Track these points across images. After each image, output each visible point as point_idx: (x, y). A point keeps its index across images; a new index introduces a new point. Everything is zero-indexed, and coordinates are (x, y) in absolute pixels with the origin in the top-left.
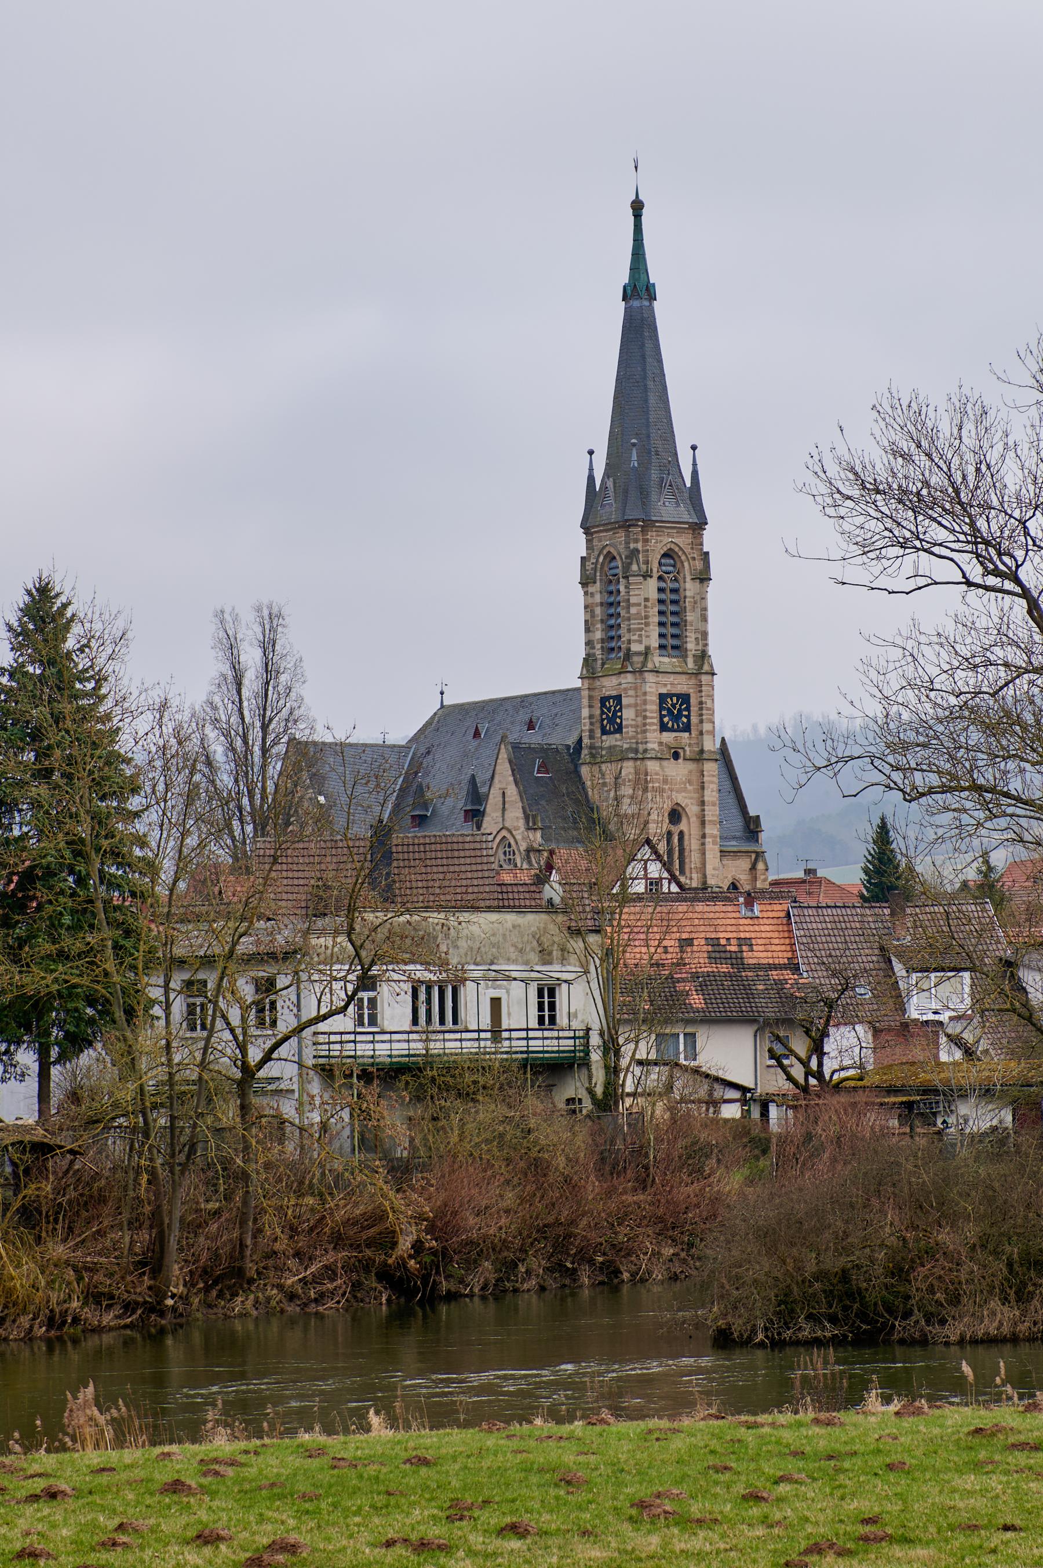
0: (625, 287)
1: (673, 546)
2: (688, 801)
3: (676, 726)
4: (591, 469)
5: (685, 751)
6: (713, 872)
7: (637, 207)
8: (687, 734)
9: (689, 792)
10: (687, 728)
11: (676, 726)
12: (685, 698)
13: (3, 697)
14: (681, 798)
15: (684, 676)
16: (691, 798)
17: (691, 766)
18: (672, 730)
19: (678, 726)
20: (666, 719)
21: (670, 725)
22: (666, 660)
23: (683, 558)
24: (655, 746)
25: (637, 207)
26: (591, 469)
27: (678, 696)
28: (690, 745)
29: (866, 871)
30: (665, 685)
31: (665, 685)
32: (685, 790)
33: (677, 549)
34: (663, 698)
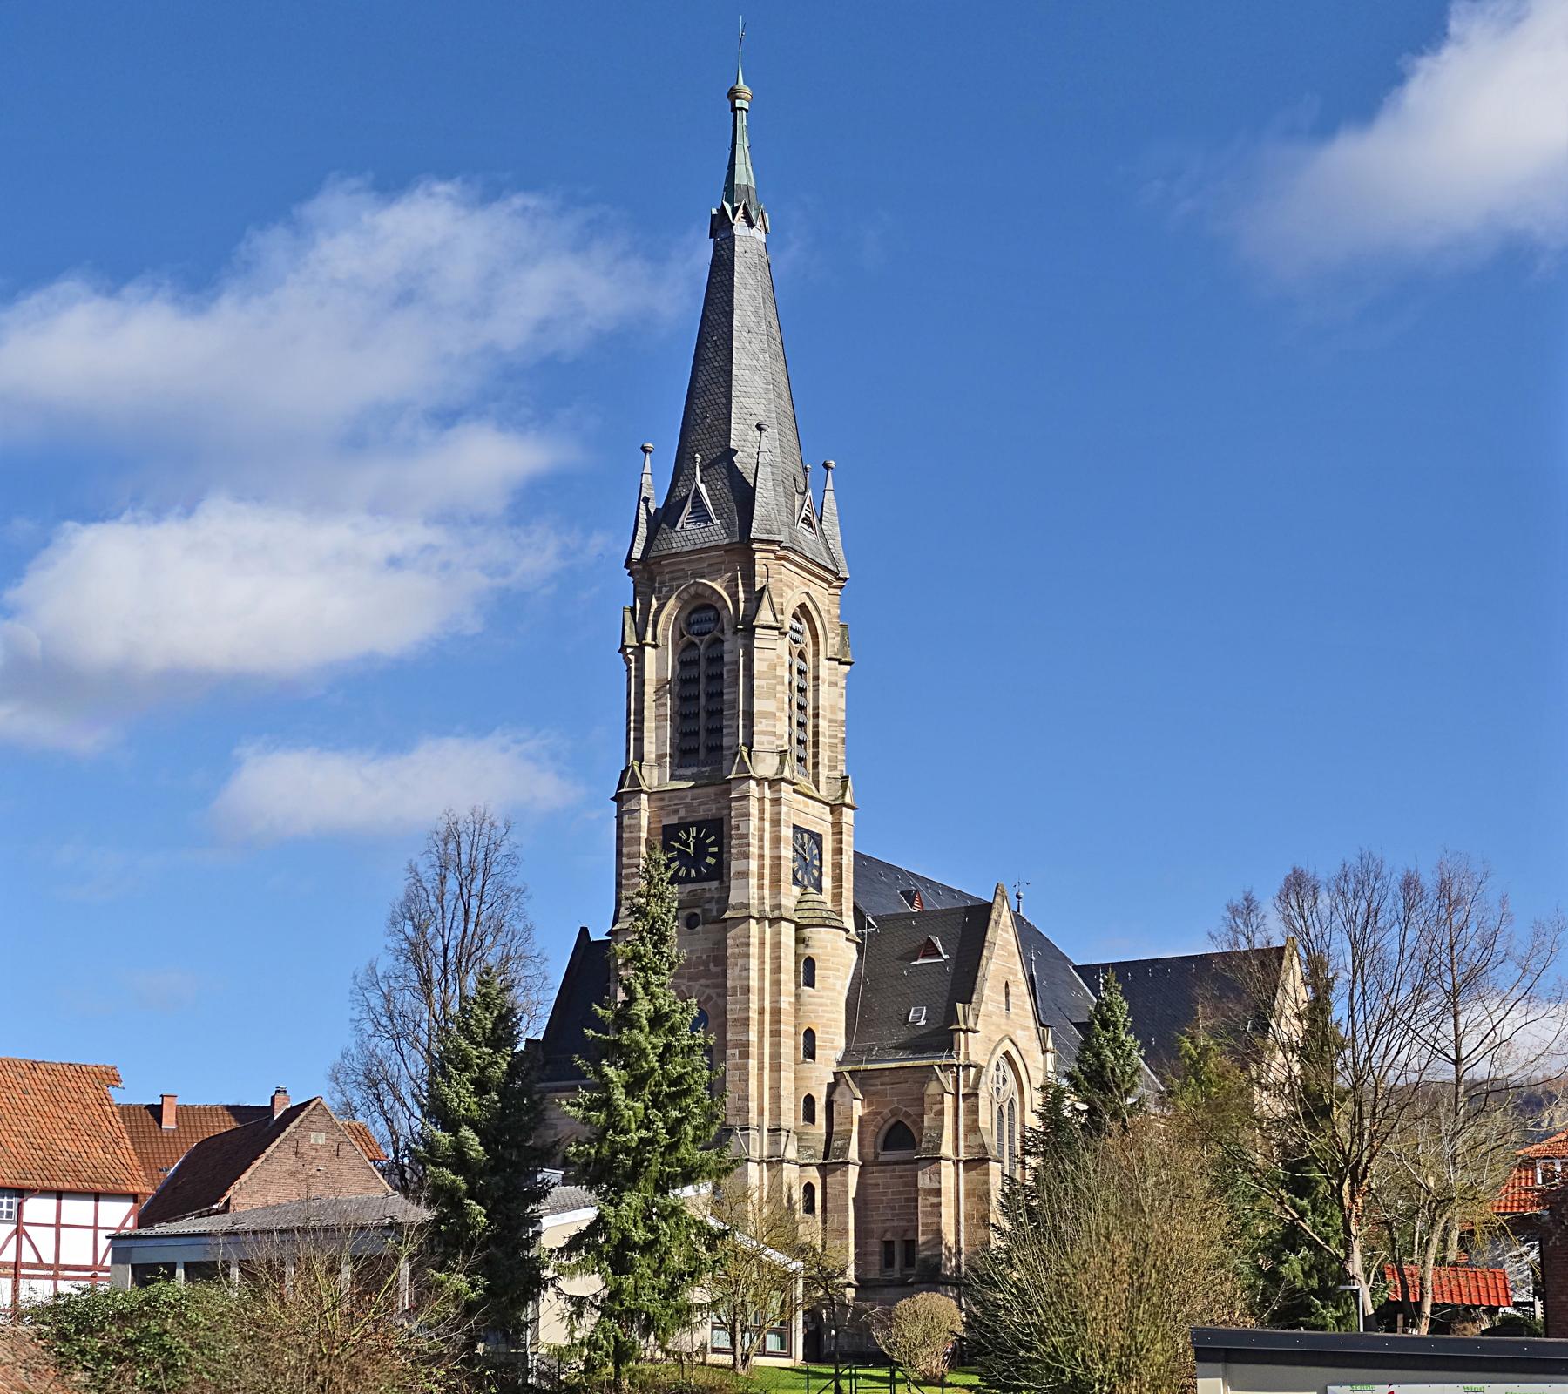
4: (963, 1386)
8: (714, 884)
11: (716, 849)
21: (682, 873)
26: (963, 1386)
30: (676, 812)
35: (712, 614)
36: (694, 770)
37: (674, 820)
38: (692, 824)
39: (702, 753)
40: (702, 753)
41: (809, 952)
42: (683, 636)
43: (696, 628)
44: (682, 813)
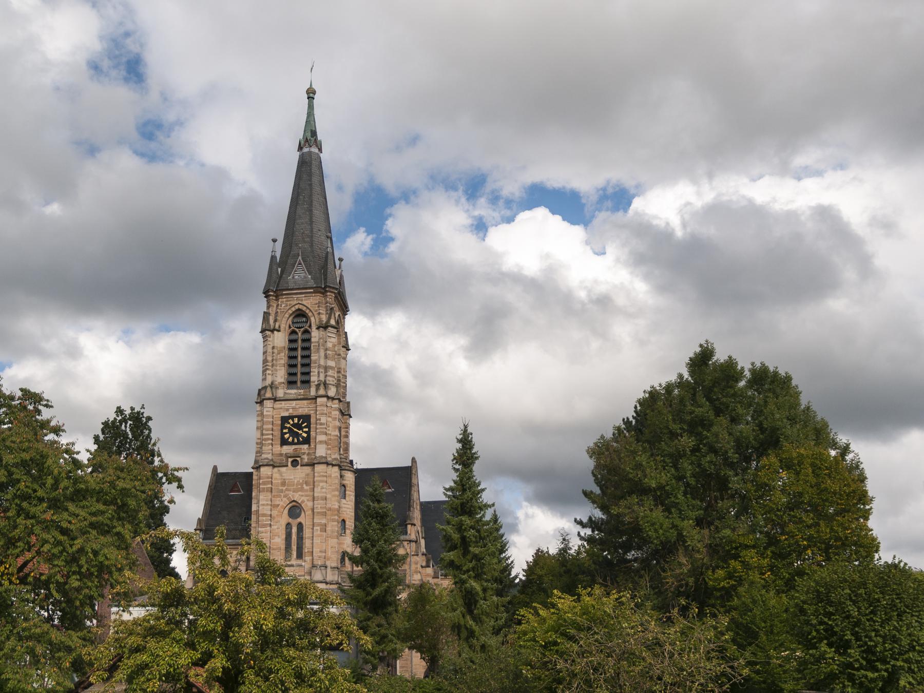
0: (754, 180)
1: (301, 307)
2: (305, 499)
3: (296, 440)
5: (302, 459)
6: (320, 554)
7: (311, 94)
8: (306, 446)
9: (307, 491)
10: (307, 441)
11: (296, 440)
12: (306, 418)
13: (412, 664)
14: (297, 497)
15: (305, 402)
16: (307, 496)
17: (308, 469)
18: (293, 443)
19: (298, 440)
20: (287, 436)
21: (291, 439)
22: (293, 391)
23: (310, 314)
24: (270, 456)
25: (311, 94)
27: (299, 417)
28: (308, 454)
29: (96, 439)
30: (287, 410)
31: (287, 410)
32: (302, 489)
33: (304, 309)
34: (284, 420)
35: (304, 319)
36: (295, 391)
37: (286, 414)
38: (296, 417)
39: (299, 383)
40: (299, 383)
41: (344, 482)
42: (290, 327)
43: (299, 325)
44: (291, 411)
